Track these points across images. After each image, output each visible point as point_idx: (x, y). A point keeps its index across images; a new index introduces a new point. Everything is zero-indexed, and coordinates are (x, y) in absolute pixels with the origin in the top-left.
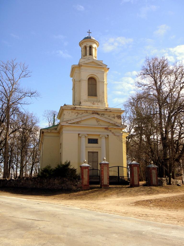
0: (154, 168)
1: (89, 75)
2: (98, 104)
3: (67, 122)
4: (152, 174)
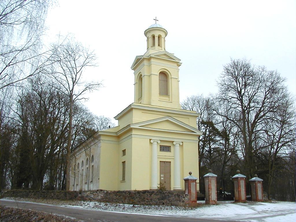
0: (259, 182)
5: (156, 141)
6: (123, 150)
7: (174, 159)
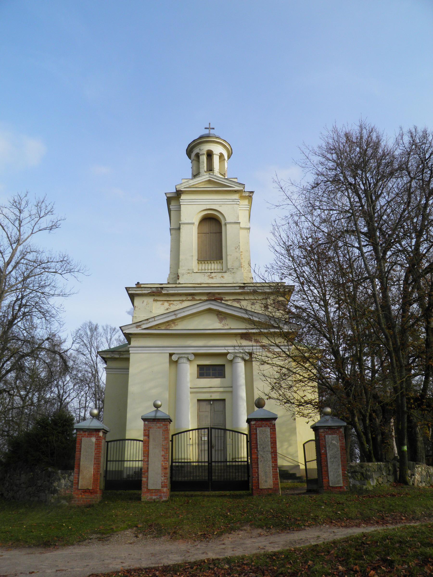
2: (222, 277)
4: (326, 451)
5: (183, 356)
7: (231, 392)
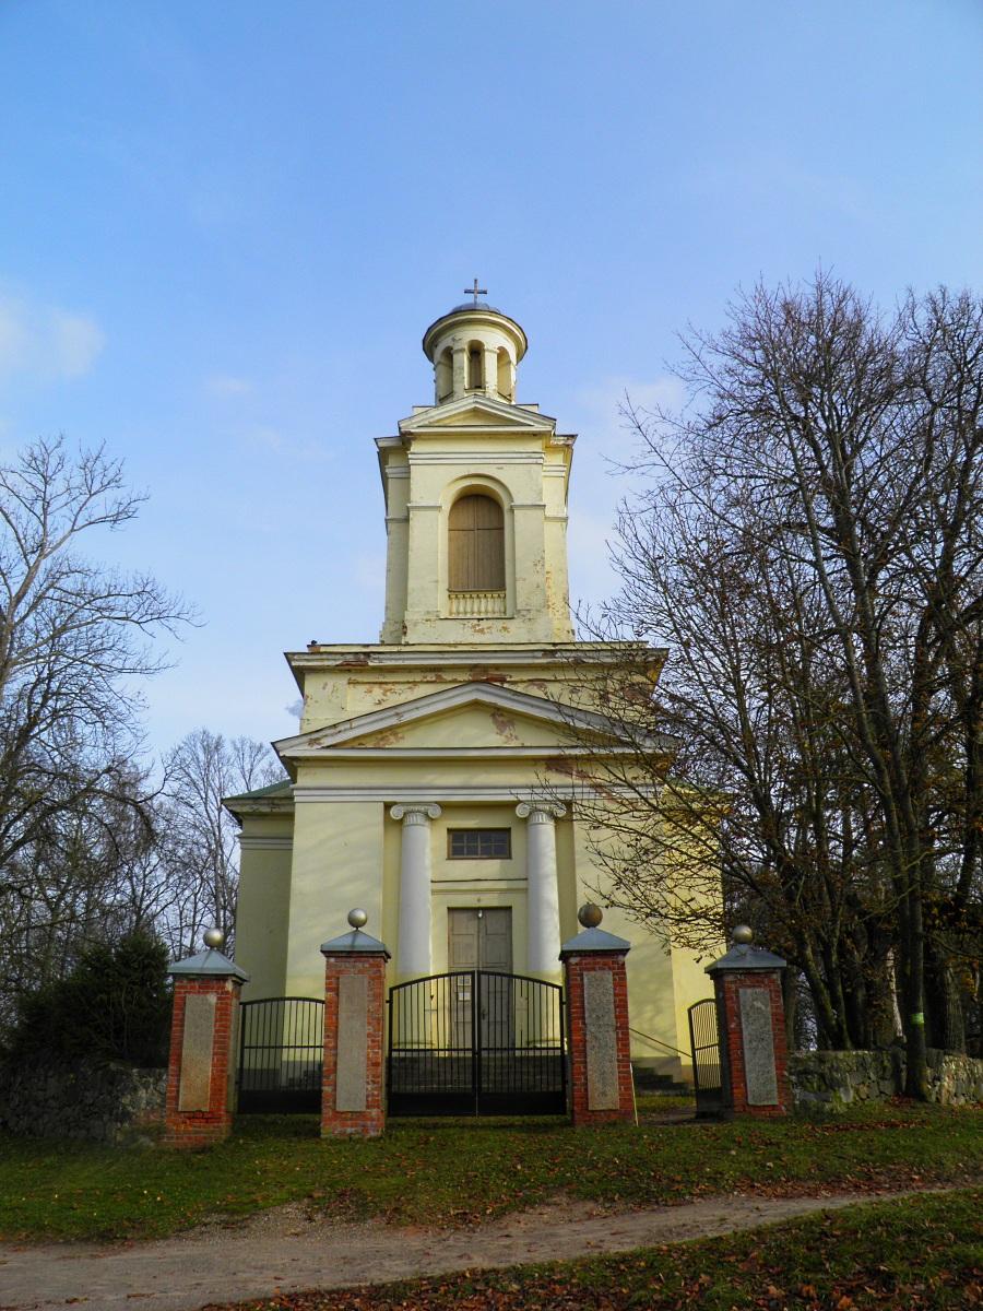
1: (457, 480)
2: (505, 629)
3: (314, 736)
5: (416, 808)
6: (508, 861)
